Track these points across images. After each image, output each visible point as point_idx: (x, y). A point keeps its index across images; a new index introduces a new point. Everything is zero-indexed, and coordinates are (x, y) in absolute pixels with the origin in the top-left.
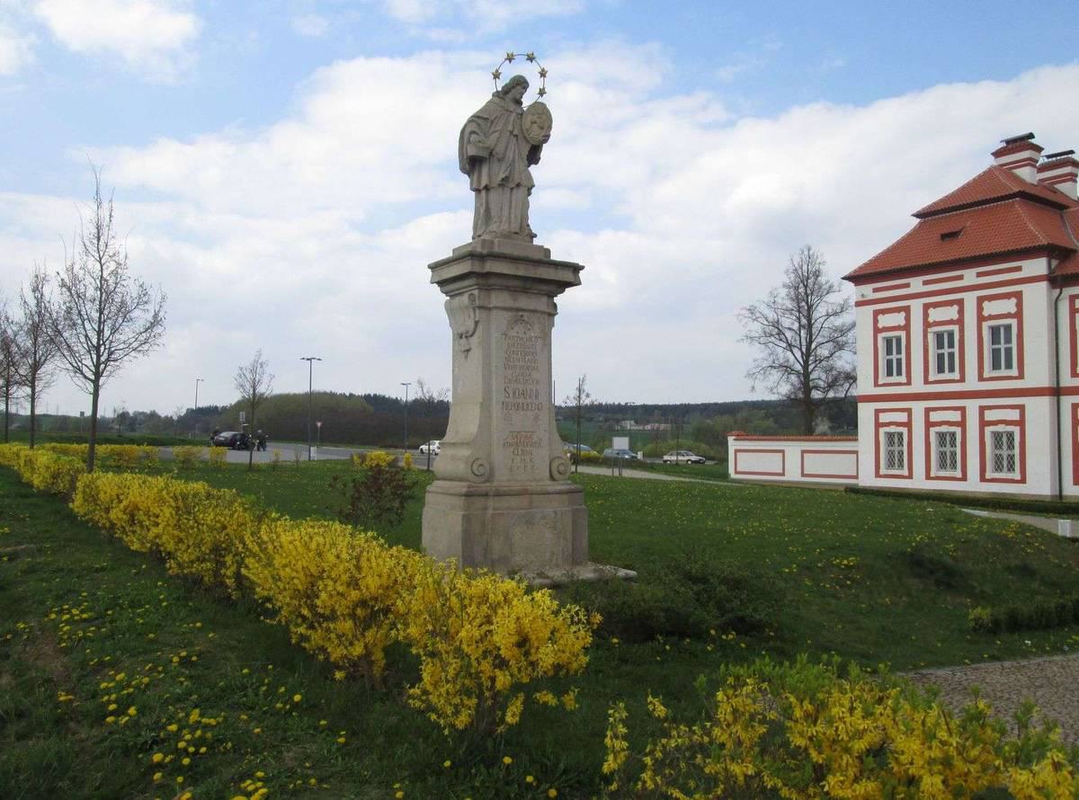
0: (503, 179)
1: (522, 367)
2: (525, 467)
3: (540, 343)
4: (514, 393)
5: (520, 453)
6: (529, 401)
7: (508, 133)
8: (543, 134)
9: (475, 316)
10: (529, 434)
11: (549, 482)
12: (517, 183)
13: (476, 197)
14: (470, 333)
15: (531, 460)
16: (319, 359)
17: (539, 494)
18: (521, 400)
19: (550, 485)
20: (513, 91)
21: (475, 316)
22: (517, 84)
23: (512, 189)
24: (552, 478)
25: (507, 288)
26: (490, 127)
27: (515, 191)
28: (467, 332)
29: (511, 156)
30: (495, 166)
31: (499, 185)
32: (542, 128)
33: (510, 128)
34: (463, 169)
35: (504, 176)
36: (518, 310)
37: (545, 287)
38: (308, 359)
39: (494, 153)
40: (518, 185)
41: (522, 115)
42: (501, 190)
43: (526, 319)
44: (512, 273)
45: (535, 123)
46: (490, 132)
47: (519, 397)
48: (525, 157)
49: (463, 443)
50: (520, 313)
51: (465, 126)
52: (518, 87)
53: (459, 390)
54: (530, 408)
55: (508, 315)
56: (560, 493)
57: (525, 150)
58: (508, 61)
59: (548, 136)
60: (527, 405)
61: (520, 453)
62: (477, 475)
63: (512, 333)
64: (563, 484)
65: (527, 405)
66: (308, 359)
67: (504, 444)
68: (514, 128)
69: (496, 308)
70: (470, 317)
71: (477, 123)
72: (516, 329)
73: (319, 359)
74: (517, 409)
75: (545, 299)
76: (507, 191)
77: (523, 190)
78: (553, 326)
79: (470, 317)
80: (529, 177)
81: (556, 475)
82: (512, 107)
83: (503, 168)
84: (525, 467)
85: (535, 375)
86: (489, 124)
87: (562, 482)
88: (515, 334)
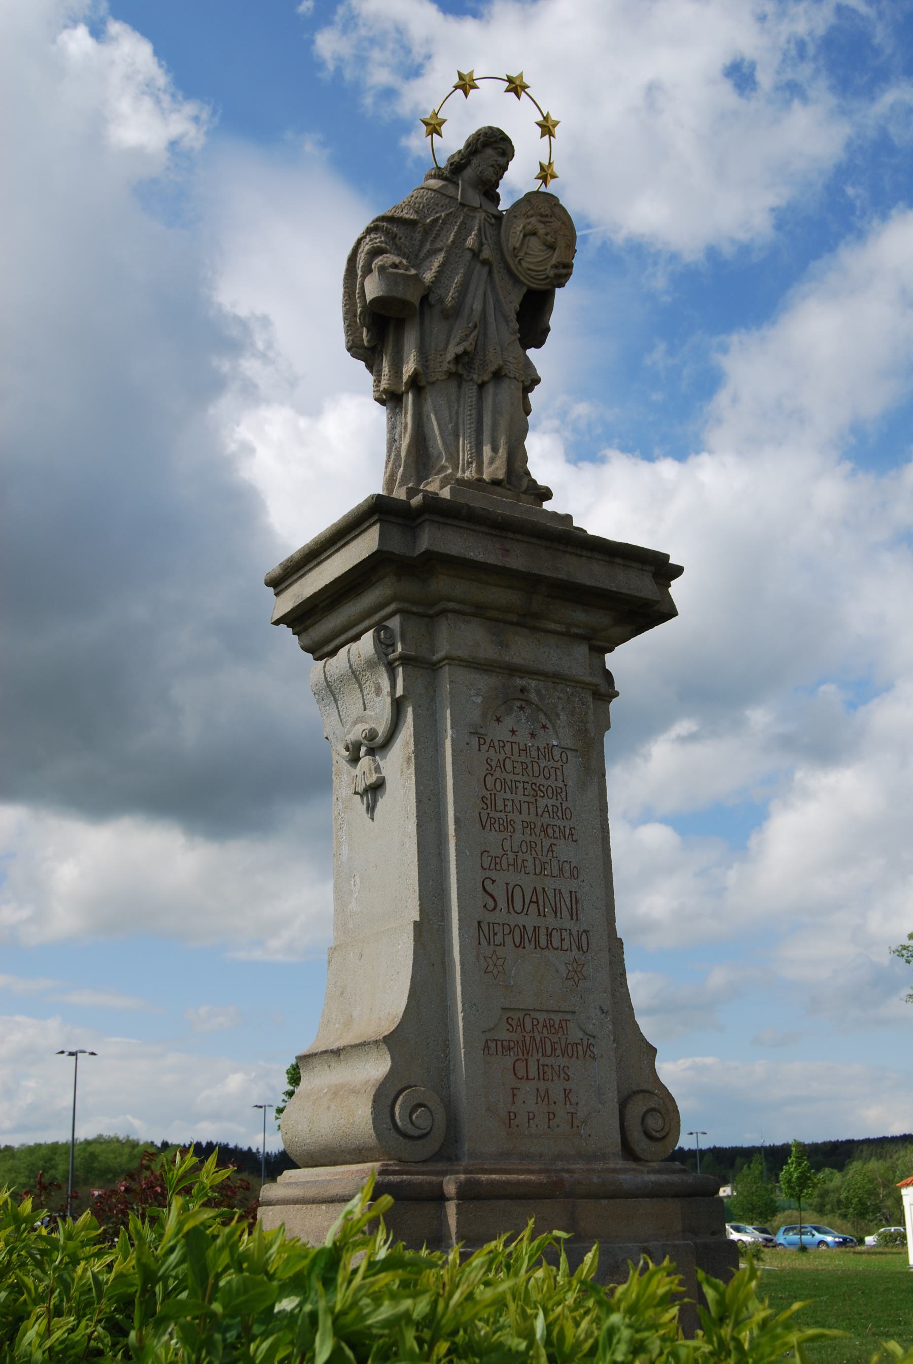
0: (458, 358)
1: (527, 825)
2: (551, 1115)
3: (572, 769)
4: (510, 900)
5: (533, 1072)
6: (551, 921)
7: (468, 255)
8: (554, 261)
9: (393, 686)
10: (557, 1018)
11: (621, 1164)
12: (492, 368)
13: (389, 419)
14: (380, 739)
15: (567, 1093)
16: (93, 1054)
17: (597, 1197)
18: (530, 921)
19: (624, 1171)
20: (475, 162)
21: (393, 686)
22: (485, 145)
23: (482, 386)
24: (628, 1152)
25: (479, 611)
26: (422, 242)
27: (490, 389)
28: (371, 735)
29: (477, 306)
30: (437, 328)
31: (451, 375)
32: (552, 247)
33: (470, 242)
34: (355, 349)
35: (460, 350)
36: (513, 670)
37: (581, 617)
38: (71, 1054)
39: (433, 299)
40: (498, 376)
41: (499, 217)
42: (452, 387)
43: (533, 697)
44: (492, 560)
45: (534, 234)
46: (422, 255)
47: (524, 911)
48: (513, 316)
49: (364, 1044)
50: (519, 682)
51: (359, 242)
52: (489, 151)
53: (353, 906)
54: (556, 942)
55: (484, 682)
56: (654, 1193)
57: (513, 301)
58: (460, 92)
59: (569, 266)
60: (549, 935)
61: (533, 1072)
62: (405, 1135)
63: (500, 732)
64: (659, 1171)
65: (549, 935)
66: (71, 1054)
67: (486, 1047)
68: (481, 244)
69: (450, 659)
70: (378, 691)
71: (387, 233)
72: (509, 722)
73: (93, 1054)
74: (520, 945)
75: (582, 650)
76: (470, 392)
77: (508, 391)
78: (608, 727)
79: (378, 691)
80: (528, 365)
81: (641, 1144)
82: (475, 199)
83: (458, 334)
84: (551, 1115)
85: (565, 850)
86: (418, 236)
87: (655, 1165)
88: (507, 737)
